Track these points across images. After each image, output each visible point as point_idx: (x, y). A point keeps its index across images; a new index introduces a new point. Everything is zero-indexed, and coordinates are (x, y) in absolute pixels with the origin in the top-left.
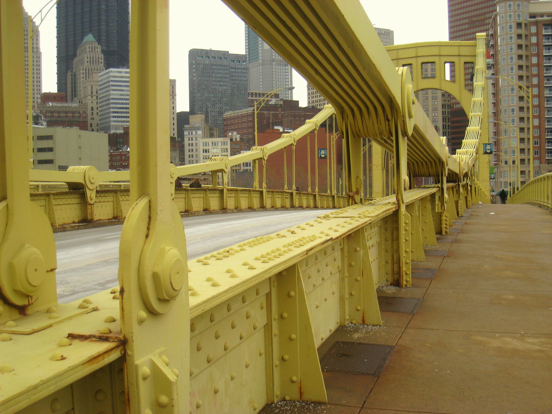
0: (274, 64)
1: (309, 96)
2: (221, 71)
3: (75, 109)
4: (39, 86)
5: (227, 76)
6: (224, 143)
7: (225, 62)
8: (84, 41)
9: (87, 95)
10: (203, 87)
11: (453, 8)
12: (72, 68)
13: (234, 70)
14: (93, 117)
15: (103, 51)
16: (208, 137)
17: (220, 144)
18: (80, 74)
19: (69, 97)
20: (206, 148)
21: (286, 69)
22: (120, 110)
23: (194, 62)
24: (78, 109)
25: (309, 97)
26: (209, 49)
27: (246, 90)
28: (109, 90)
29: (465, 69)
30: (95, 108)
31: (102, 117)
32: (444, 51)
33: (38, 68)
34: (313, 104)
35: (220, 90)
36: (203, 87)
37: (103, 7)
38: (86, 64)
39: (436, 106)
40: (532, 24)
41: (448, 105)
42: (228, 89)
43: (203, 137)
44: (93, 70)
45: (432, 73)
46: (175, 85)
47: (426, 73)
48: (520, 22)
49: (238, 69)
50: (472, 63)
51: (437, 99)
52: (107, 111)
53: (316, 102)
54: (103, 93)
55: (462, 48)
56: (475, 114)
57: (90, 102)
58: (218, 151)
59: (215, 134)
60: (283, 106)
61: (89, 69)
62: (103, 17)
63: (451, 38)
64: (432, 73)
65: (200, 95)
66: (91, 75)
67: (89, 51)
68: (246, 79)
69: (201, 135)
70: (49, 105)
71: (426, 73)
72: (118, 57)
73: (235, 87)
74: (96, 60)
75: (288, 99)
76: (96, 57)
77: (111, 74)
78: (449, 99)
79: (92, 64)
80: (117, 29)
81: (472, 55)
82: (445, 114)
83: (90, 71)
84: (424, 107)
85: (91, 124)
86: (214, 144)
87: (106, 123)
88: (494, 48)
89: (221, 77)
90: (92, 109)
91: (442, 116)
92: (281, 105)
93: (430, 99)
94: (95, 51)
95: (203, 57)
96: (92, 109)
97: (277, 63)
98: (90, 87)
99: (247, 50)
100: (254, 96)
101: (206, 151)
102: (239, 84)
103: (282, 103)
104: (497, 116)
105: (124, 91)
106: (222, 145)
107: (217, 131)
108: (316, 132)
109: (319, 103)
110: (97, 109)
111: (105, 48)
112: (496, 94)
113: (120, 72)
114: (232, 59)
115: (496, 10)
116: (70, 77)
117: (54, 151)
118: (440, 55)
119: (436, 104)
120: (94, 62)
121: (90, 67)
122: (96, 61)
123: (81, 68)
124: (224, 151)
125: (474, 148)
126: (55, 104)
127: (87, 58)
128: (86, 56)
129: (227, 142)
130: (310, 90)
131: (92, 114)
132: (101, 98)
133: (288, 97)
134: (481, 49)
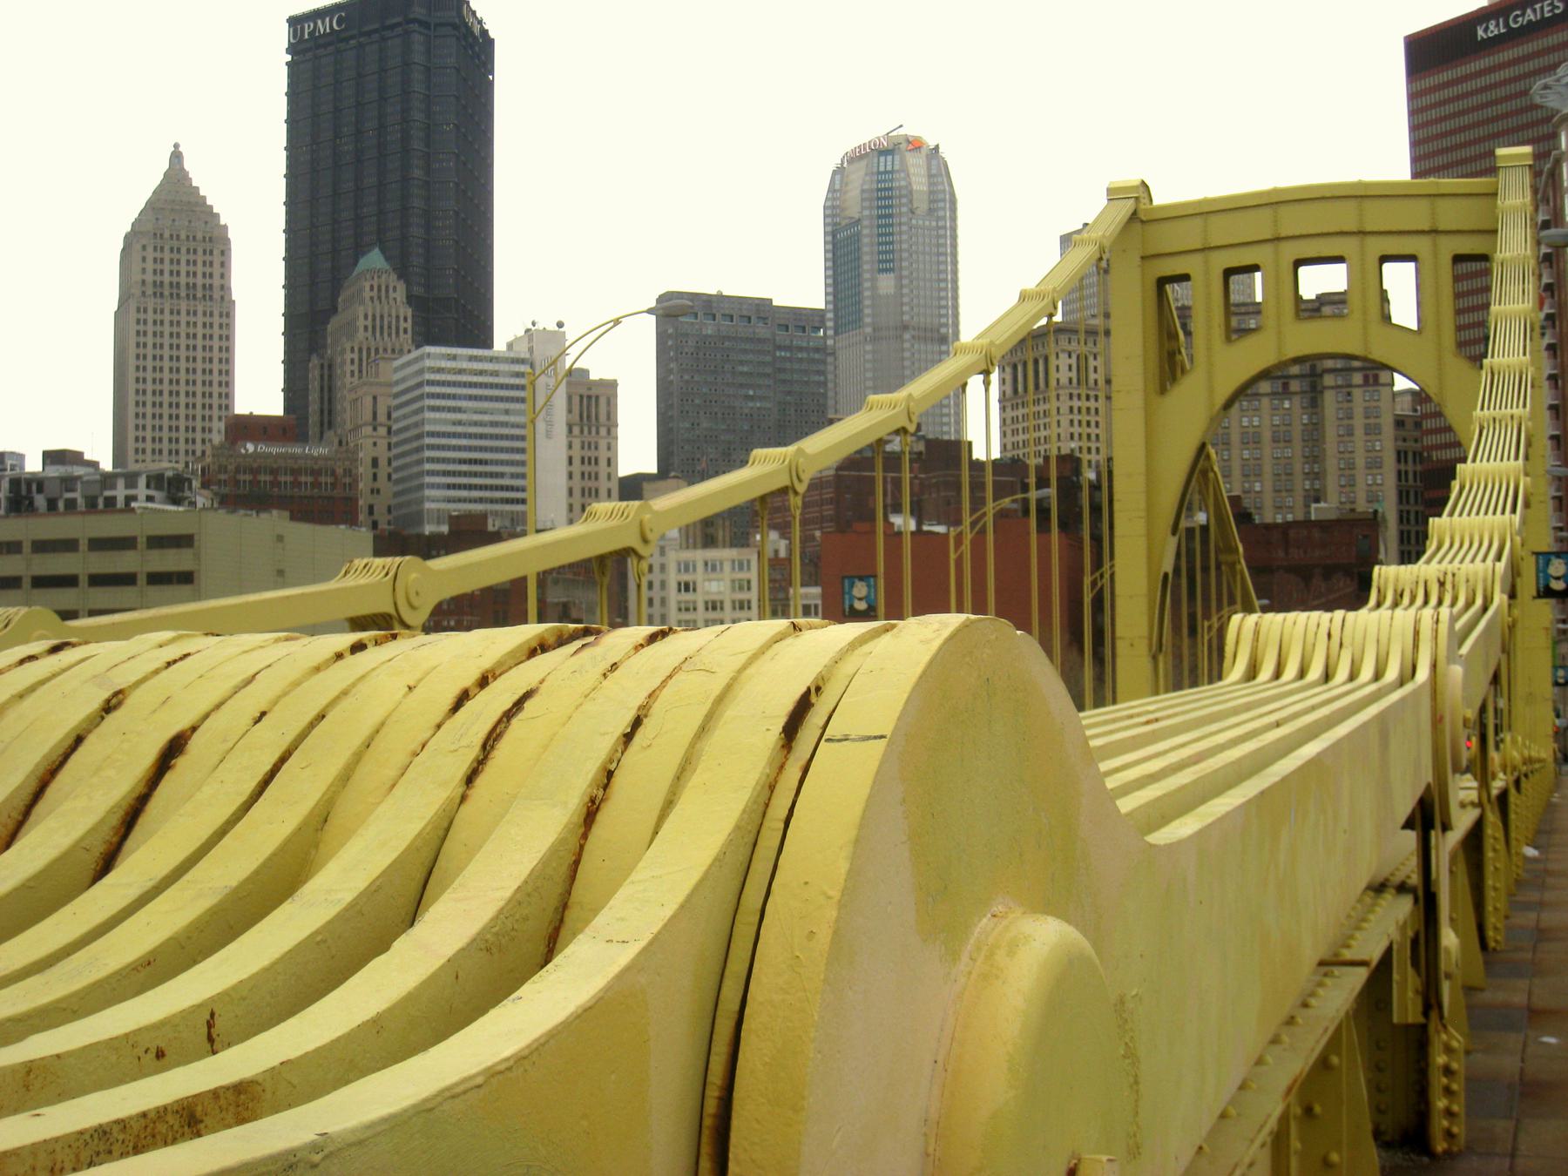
0: (907, 336)
2: (750, 357)
3: (299, 461)
4: (227, 395)
5: (768, 370)
6: (741, 565)
7: (762, 331)
8: (355, 273)
9: (360, 422)
10: (697, 401)
11: (1422, 133)
12: (325, 346)
13: (788, 355)
14: (377, 485)
15: (410, 300)
16: (699, 545)
17: (727, 567)
18: (343, 363)
19: (313, 430)
20: (685, 577)
22: (464, 468)
23: (670, 331)
24: (329, 462)
26: (714, 292)
28: (421, 410)
29: (1457, 279)
30: (383, 462)
31: (400, 487)
32: (1377, 218)
33: (224, 344)
34: (1015, 453)
35: (746, 411)
36: (697, 401)
37: (417, 173)
38: (361, 334)
39: (1379, 454)
41: (1414, 454)
42: (769, 409)
43: (684, 545)
44: (381, 350)
46: (616, 396)
49: (801, 349)
50: (1485, 258)
51: (1380, 434)
52: (415, 470)
54: (405, 417)
55: (1443, 204)
56: (1497, 413)
57: (369, 445)
58: (722, 589)
59: (720, 538)
60: (924, 457)
61: (369, 349)
62: (417, 203)
63: (1415, 175)
65: (687, 426)
66: (373, 365)
67: (372, 298)
68: (822, 378)
69: (675, 540)
70: (245, 448)
72: (456, 316)
73: (790, 403)
74: (390, 323)
75: (946, 437)
76: (390, 315)
77: (428, 363)
78: (1417, 434)
79: (378, 334)
80: (455, 237)
82: (1407, 480)
83: (373, 354)
84: (1342, 456)
85: (371, 509)
86: (710, 567)
87: (409, 503)
89: (750, 374)
90: (375, 462)
91: (1398, 486)
92: (920, 453)
93: (1359, 432)
94: (387, 297)
95: (696, 316)
96: (375, 462)
98: (368, 401)
99: (830, 298)
101: (687, 587)
102: (801, 393)
103: (921, 447)
105: (465, 412)
106: (733, 569)
107: (727, 530)
108: (795, 502)
110: (389, 463)
111: (418, 290)
112: (1561, 409)
113: (454, 358)
114: (782, 322)
115: (1558, 147)
116: (317, 373)
117: (196, 581)
118: (1362, 233)
119: (1378, 448)
120: (386, 327)
121: (381, 344)
122: (390, 327)
123: (348, 346)
124: (741, 588)
125: (1498, 558)
126: (263, 448)
127: (366, 317)
128: (361, 311)
129: (749, 561)
130: (1008, 410)
131: (375, 477)
132: (400, 431)
133: (949, 433)
134: (1515, 196)
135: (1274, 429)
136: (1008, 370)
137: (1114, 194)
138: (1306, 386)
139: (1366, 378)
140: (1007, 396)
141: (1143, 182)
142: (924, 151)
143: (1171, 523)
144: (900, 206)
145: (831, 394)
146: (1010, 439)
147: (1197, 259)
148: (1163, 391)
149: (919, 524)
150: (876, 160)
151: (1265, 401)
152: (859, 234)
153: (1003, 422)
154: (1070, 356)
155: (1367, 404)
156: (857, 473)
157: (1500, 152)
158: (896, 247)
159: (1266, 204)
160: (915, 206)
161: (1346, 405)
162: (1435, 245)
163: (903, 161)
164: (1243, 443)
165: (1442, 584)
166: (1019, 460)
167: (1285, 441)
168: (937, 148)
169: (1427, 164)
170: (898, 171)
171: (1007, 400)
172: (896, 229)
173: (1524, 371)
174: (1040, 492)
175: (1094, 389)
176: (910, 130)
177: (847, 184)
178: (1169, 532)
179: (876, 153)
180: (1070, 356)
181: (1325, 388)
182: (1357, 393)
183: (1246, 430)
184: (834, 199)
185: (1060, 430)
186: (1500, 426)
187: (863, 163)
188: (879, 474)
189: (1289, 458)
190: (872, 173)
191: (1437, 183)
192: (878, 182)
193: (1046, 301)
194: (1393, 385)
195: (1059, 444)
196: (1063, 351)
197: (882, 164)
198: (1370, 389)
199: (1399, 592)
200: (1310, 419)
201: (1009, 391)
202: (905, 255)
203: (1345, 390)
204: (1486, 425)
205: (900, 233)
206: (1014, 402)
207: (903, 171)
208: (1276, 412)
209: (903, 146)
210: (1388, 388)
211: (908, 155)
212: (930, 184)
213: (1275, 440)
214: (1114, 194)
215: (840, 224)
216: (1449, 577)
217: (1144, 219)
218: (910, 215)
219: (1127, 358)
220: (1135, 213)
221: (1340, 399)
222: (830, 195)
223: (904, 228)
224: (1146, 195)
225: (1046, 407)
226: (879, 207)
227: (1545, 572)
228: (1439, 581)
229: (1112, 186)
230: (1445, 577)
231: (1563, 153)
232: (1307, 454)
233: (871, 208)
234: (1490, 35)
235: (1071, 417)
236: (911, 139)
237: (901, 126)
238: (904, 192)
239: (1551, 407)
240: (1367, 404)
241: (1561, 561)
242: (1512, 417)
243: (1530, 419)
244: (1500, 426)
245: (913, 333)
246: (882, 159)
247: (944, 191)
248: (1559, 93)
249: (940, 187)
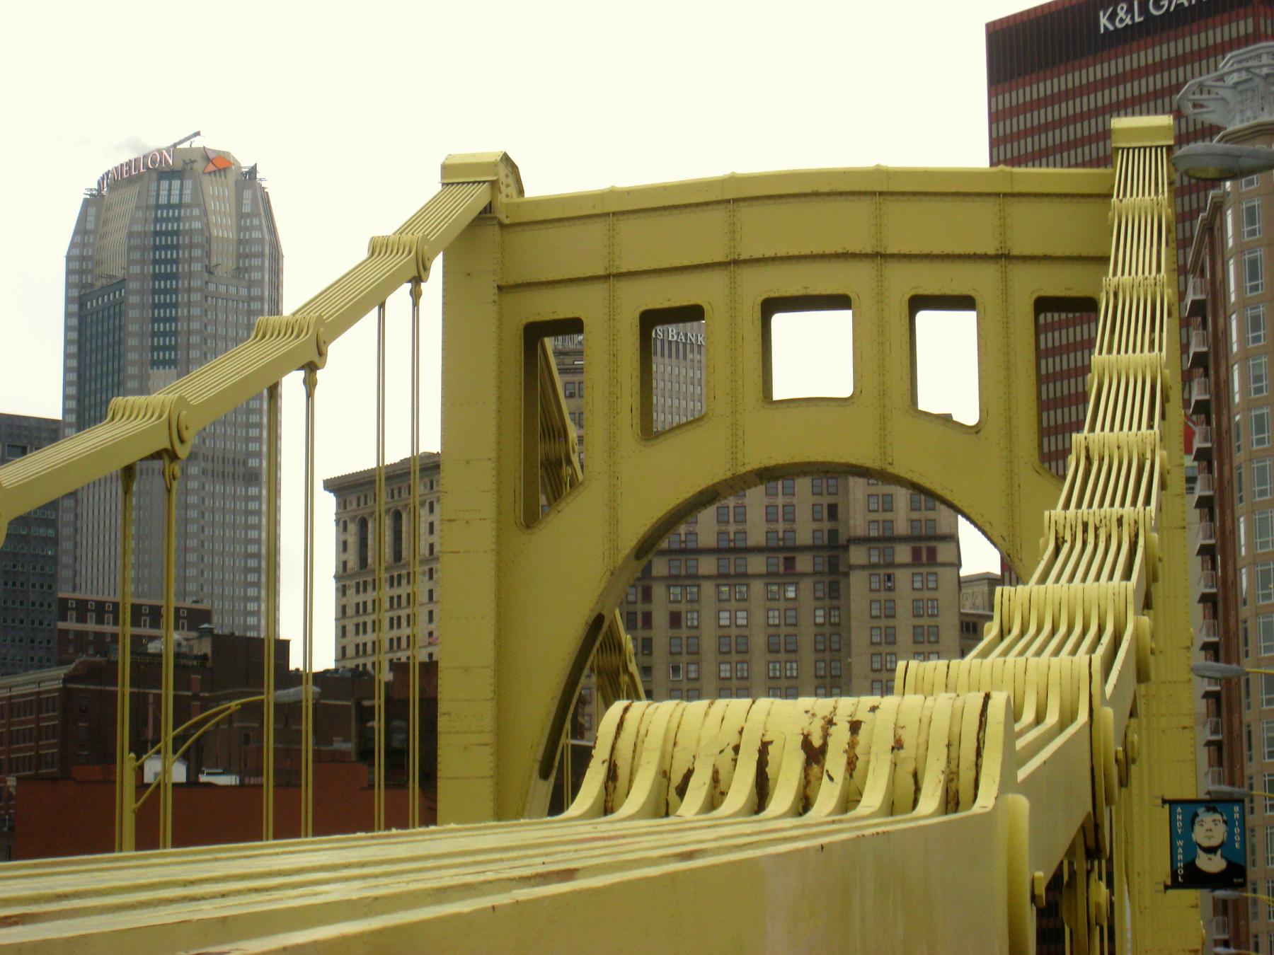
1: (346, 622)
21: (248, 498)
25: (344, 628)
27: (50, 581)
34: (361, 661)
45: (916, 515)
47: (888, 516)
51: (937, 642)
55: (1019, 210)
60: (209, 664)
64: (916, 515)
68: (51, 532)
71: (888, 516)
81: (1084, 252)
84: (877, 676)
88: (1212, 372)
92: (205, 657)
97: (209, 466)
99: (73, 404)
100: (92, 616)
102: (16, 554)
103: (205, 647)
104: (1230, 712)
118: (880, 256)
130: (351, 592)
133: (258, 627)
135: (772, 631)
136: (352, 527)
137: (454, 174)
138: (822, 564)
139: (916, 554)
140: (348, 570)
141: (506, 159)
142: (232, 177)
143: (539, 755)
144: (191, 260)
145: (66, 559)
146: (352, 640)
147: (597, 293)
148: (531, 519)
149: (193, 771)
150: (153, 186)
151: (757, 587)
152: (121, 302)
153: (342, 612)
155: (918, 595)
156: (99, 688)
157: (1120, 123)
158: (183, 326)
159: (719, 202)
160: (214, 262)
161: (883, 595)
162: (1005, 281)
163: (198, 191)
164: (720, 652)
165: (814, 755)
166: (365, 672)
167: (787, 651)
168: (253, 170)
170: (188, 206)
171: (351, 577)
172: (183, 298)
173: (1148, 455)
174: (281, 692)
176: (211, 141)
177: (105, 222)
178: (536, 774)
179: (154, 175)
181: (851, 567)
182: (902, 576)
183: (726, 632)
184: (84, 245)
186: (1096, 537)
187: (136, 189)
188: (124, 689)
189: (792, 677)
190: (147, 208)
191: (1012, 173)
192: (157, 220)
193: (302, 338)
194: (959, 565)
197: (164, 193)
198: (924, 570)
199: (676, 779)
200: (827, 616)
201: (353, 563)
202: (195, 339)
203: (882, 572)
204: (1068, 537)
205: (189, 305)
206: (361, 580)
207: (198, 205)
208: (773, 604)
209: (199, 166)
210: (948, 570)
211: (206, 180)
212: (240, 229)
213: (772, 649)
214: (454, 174)
215: (92, 285)
216: (840, 734)
217: (507, 221)
218: (206, 276)
219: (468, 462)
220: (489, 209)
221: (875, 586)
222: (78, 239)
223: (196, 297)
224: (511, 180)
226: (155, 262)
227: (1187, 836)
228: (806, 744)
229: (451, 161)
230: (826, 735)
231: (1228, 194)
232: (822, 673)
233: (143, 262)
234: (1119, 26)
236: (211, 156)
237: (198, 134)
238: (197, 239)
239: (1204, 598)
240: (918, 595)
241: (1217, 816)
242: (1120, 521)
243: (1158, 528)
244: (1096, 537)
245: (203, 464)
246: (164, 184)
247: (261, 241)
248: (1223, 99)
249: (256, 235)
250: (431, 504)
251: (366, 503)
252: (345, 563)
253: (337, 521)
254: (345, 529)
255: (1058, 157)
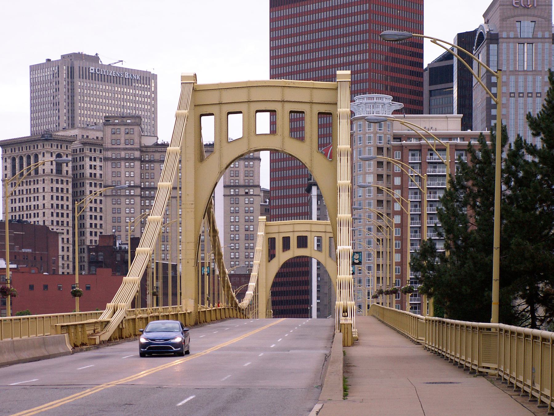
29: (291, 121)
32: (256, 95)
40: (396, 148)
48: (382, 146)
53: (19, 210)
63: (272, 77)
109: (26, 212)
136: (9, 161)
146: (10, 206)
154: (52, 156)
157: (338, 72)
169: (280, 71)
175: (65, 177)
180: (52, 156)
185: (45, 202)
195: (44, 210)
196: (47, 152)
225: (36, 186)
235: (52, 194)
250: (44, 153)
251: (15, 151)
252: (6, 175)
253: (2, 158)
254: (6, 161)
255: (293, 76)
